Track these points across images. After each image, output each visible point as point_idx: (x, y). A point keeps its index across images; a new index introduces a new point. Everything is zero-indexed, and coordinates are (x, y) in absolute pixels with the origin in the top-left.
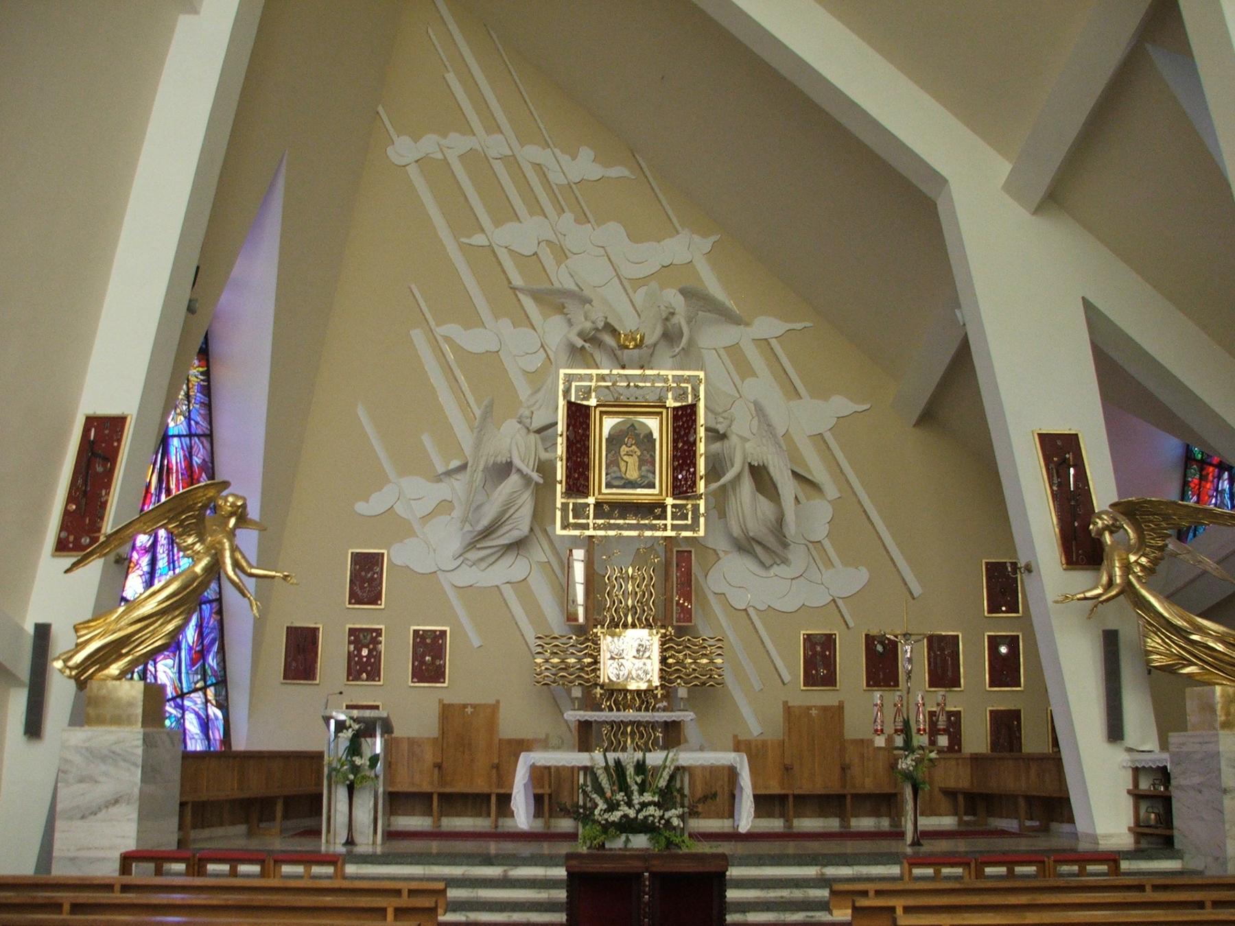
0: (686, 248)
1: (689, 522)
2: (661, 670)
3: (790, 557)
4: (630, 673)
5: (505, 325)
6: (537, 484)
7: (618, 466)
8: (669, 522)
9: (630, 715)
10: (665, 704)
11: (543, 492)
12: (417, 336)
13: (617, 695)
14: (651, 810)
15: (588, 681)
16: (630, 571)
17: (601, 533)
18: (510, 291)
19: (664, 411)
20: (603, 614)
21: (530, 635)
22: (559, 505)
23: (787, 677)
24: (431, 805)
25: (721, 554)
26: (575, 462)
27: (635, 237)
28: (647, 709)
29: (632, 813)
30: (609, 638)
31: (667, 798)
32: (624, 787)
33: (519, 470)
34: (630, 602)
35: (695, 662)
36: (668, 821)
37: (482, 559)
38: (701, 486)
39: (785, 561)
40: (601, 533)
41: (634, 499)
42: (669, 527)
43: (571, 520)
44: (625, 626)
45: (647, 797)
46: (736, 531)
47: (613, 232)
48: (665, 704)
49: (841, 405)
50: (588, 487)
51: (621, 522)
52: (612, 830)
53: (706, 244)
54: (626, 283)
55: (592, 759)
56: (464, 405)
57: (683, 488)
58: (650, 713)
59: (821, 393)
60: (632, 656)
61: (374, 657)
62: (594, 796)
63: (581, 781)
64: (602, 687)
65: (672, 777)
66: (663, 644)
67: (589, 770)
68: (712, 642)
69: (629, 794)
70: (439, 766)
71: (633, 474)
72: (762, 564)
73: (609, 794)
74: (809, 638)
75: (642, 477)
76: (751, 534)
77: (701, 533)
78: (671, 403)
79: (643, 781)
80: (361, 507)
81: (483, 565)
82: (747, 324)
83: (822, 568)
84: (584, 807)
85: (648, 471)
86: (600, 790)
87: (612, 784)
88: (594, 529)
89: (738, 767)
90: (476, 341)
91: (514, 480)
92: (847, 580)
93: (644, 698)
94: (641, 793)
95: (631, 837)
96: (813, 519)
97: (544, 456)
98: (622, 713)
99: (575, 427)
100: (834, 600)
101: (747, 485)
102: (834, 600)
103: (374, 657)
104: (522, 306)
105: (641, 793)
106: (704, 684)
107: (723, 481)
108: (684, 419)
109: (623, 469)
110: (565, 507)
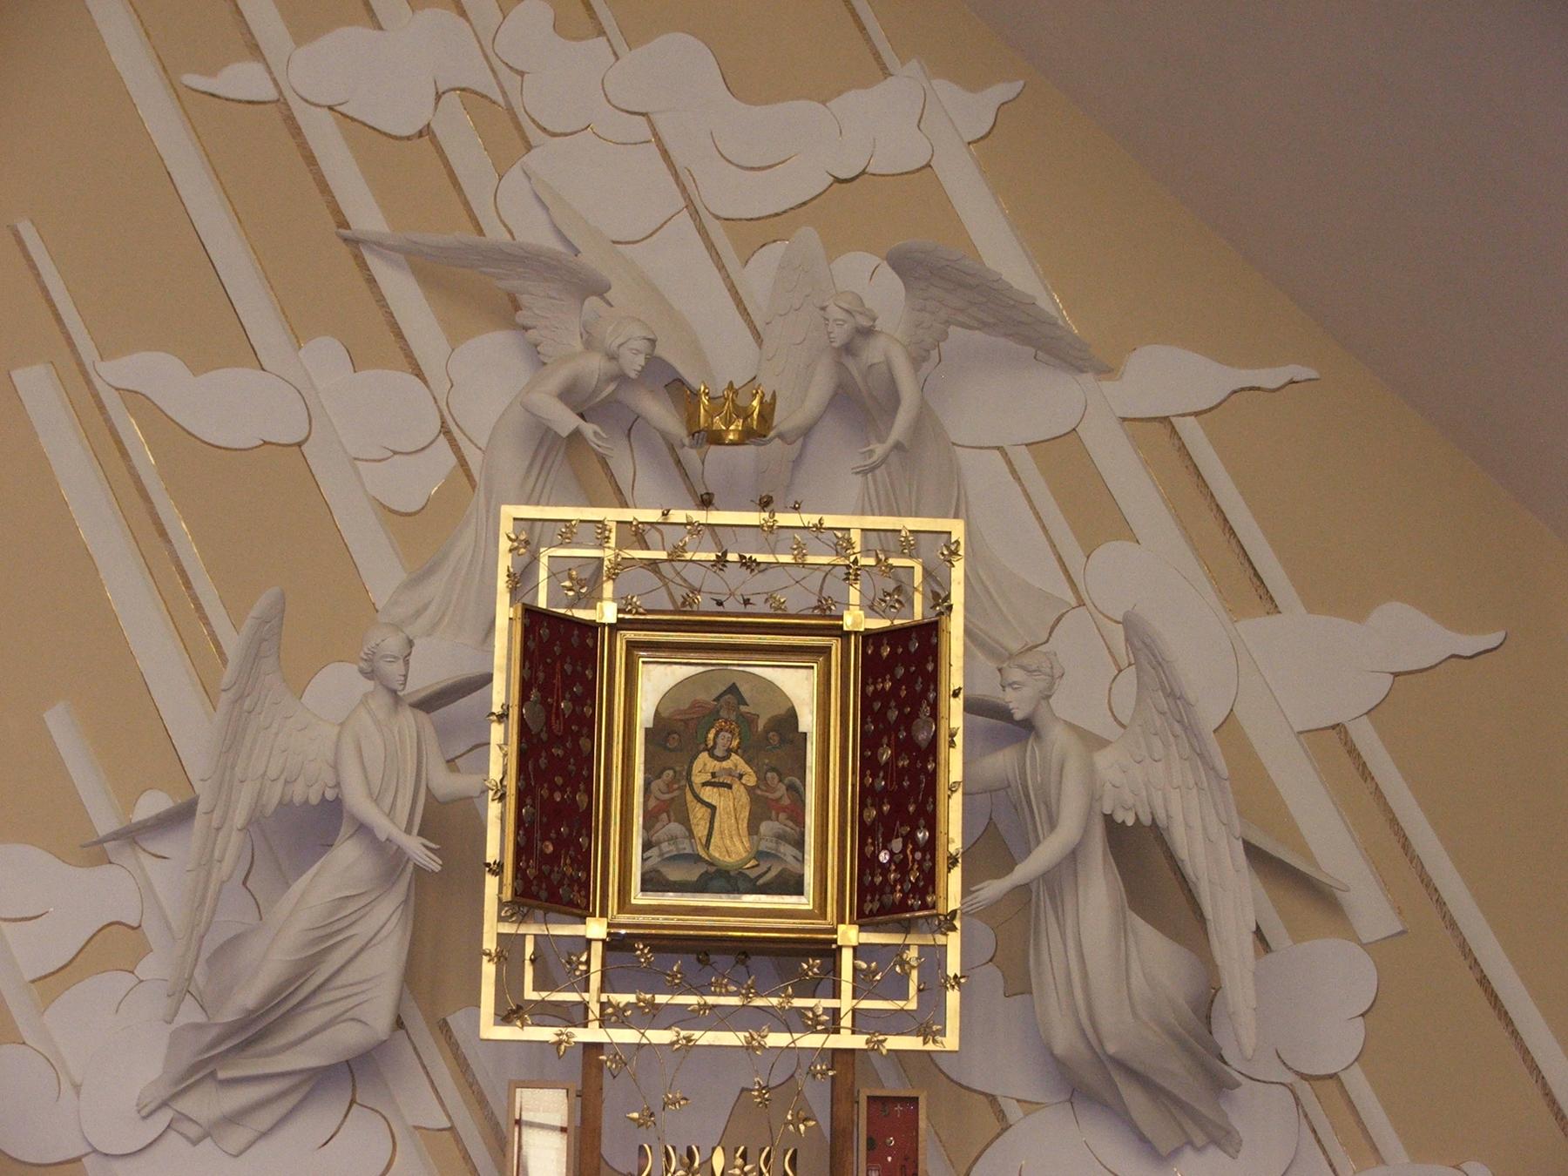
0: (910, 121)
3: (1237, 1123)
5: (325, 357)
7: (685, 821)
8: (846, 1003)
11: (438, 899)
12: (36, 385)
19: (835, 644)
22: (490, 944)
33: (363, 829)
37: (234, 1119)
38: (952, 886)
42: (846, 1021)
43: (530, 994)
47: (679, 67)
49: (1409, 635)
50: (585, 886)
53: (975, 110)
54: (716, 230)
56: (201, 650)
57: (892, 888)
59: (1340, 592)
71: (731, 847)
75: (760, 855)
76: (1111, 1048)
81: (238, 1137)
82: (1106, 371)
88: (604, 1022)
90: (227, 408)
91: (347, 854)
97: (446, 783)
99: (546, 690)
101: (1099, 890)
107: (1024, 871)
108: (898, 672)
109: (700, 831)
110: (509, 949)
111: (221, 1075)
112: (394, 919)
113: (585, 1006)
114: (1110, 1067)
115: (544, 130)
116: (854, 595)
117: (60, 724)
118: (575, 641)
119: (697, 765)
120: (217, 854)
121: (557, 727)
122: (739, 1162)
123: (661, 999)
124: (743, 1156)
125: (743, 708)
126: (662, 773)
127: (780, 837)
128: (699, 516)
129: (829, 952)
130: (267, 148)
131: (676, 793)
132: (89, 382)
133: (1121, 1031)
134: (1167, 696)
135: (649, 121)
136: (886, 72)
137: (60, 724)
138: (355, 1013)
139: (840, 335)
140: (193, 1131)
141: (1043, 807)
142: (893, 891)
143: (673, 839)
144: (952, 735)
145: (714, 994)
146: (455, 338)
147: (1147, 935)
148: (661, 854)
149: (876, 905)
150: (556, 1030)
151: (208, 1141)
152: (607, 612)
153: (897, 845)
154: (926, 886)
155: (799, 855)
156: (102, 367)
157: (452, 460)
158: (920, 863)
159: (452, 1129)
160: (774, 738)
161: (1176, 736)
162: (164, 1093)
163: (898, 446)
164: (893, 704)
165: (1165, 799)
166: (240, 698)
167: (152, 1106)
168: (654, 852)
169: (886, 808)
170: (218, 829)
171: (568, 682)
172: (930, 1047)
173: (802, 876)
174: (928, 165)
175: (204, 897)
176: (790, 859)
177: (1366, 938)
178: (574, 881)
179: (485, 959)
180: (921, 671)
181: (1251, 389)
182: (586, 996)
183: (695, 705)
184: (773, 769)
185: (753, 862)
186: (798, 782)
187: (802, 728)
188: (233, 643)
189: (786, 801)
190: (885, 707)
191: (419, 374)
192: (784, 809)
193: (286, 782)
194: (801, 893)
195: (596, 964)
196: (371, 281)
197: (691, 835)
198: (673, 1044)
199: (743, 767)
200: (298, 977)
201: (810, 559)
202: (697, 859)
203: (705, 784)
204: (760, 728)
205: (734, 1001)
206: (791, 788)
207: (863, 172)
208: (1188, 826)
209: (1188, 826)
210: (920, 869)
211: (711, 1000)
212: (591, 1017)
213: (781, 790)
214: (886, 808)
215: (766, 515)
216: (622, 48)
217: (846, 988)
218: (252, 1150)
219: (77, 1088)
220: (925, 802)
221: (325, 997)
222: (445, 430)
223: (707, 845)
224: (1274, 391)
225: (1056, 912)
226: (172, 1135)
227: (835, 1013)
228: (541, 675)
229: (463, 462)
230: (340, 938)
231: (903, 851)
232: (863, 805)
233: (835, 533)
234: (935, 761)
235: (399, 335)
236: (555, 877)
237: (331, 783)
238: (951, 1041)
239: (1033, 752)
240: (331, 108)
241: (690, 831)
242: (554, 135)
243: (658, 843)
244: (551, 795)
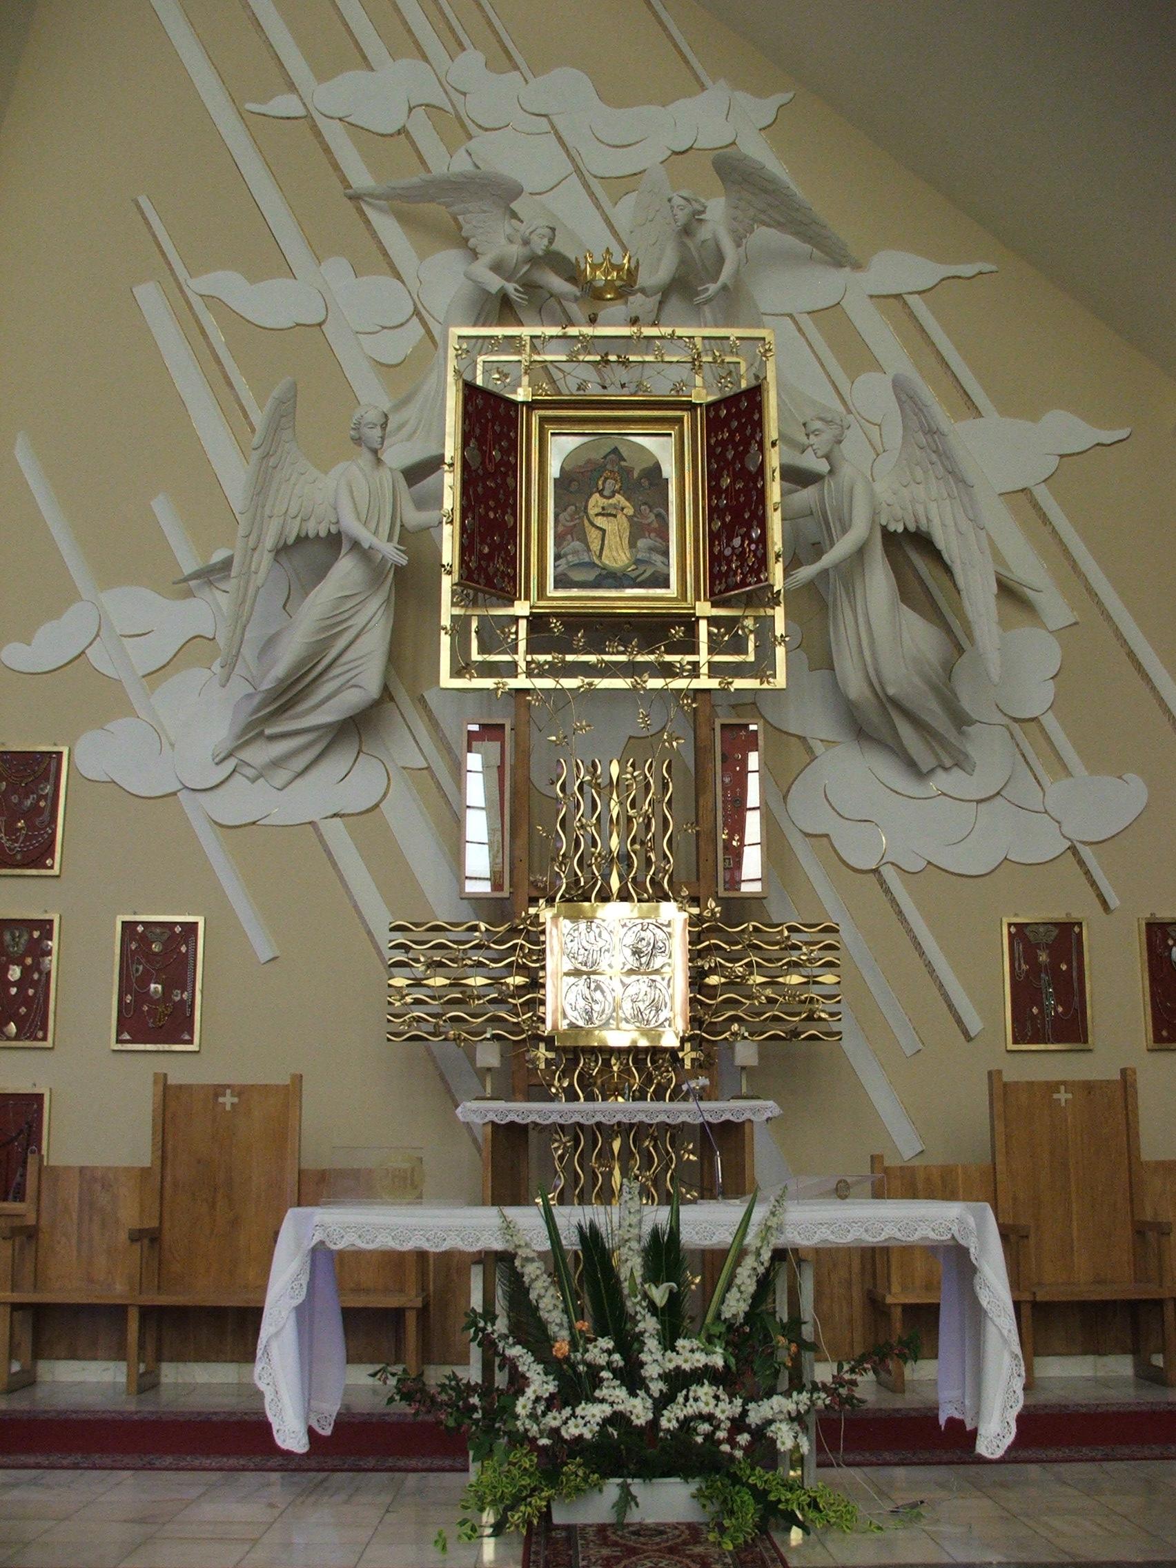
0: (725, 117)
1: (751, 658)
2: (693, 1001)
3: (970, 749)
4: (617, 1007)
5: (337, 271)
6: (398, 569)
7: (584, 540)
8: (703, 657)
9: (618, 1109)
10: (703, 1081)
11: (409, 585)
12: (149, 296)
13: (583, 1062)
14: (704, 1397)
15: (516, 1029)
16: (615, 769)
17: (547, 683)
18: (349, 204)
19: (686, 416)
20: (544, 869)
21: (380, 918)
22: (446, 621)
23: (974, 1024)
24: (123, 1332)
25: (819, 748)
26: (484, 519)
27: (614, 93)
28: (658, 1096)
29: (639, 1409)
30: (566, 925)
31: (754, 1355)
32: (610, 1317)
33: (356, 545)
34: (614, 843)
35: (772, 984)
36: (760, 1434)
37: (276, 763)
38: (777, 575)
39: (961, 762)
40: (547, 683)
41: (623, 608)
42: (704, 670)
43: (475, 656)
44: (605, 897)
45: (690, 1354)
46: (855, 687)
47: (568, 90)
48: (703, 1081)
49: (1066, 430)
50: (513, 579)
51: (592, 658)
52: (573, 1468)
53: (766, 109)
54: (594, 183)
55: (508, 1228)
56: (234, 412)
57: (733, 567)
58: (666, 1105)
59: (1022, 403)
60: (617, 972)
61: (34, 984)
62: (516, 1351)
63: (476, 1301)
64: (549, 1041)
65: (765, 1284)
66: (695, 939)
67: (501, 1263)
68: (810, 934)
69: (628, 1345)
70: (149, 1238)
71: (617, 556)
72: (911, 766)
73: (561, 1348)
74: (1020, 933)
75: (638, 562)
76: (891, 691)
77: (780, 681)
78: (701, 394)
79: (674, 1298)
80: (18, 656)
81: (282, 776)
82: (857, 266)
83: (1045, 779)
84: (486, 1389)
85: (651, 549)
86: (529, 1328)
87: (573, 1311)
88: (529, 674)
89: (972, 1245)
90: (271, 303)
91: (346, 568)
92: (1102, 804)
93: (647, 1060)
94: (668, 1344)
95: (636, 1486)
96: (1021, 666)
97: (414, 517)
98: (599, 1105)
99: (481, 441)
100: (1073, 849)
101: (879, 581)
102: (1073, 849)
103: (34, 984)
104: (374, 235)
105: (668, 1344)
106: (795, 1034)
107: (827, 560)
108: (733, 425)
109: (595, 546)
110: (459, 626)
111: (268, 732)
112: (380, 613)
113: (515, 664)
114: (888, 706)
115: (480, 127)
116: (698, 380)
117: (161, 507)
118: (502, 410)
119: (592, 502)
120: (253, 569)
121: (491, 468)
122: (630, 769)
123: (569, 658)
124: (633, 765)
125: (623, 463)
127: (651, 549)
128: (588, 331)
129: (690, 622)
130: (300, 145)
132: (182, 291)
133: (900, 679)
134: (925, 434)
136: (703, 87)
137: (161, 507)
139: (682, 216)
140: (250, 772)
141: (838, 524)
142: (735, 574)
143: (575, 552)
144: (774, 471)
145: (608, 653)
146: (422, 257)
147: (910, 617)
148: (568, 562)
149: (723, 587)
150: (496, 680)
151: (262, 780)
152: (522, 395)
153: (737, 542)
154: (760, 567)
155: (665, 560)
156: (191, 282)
157: (423, 331)
158: (755, 552)
159: (428, 768)
160: (645, 483)
161: (932, 464)
162: (229, 745)
163: (725, 288)
165: (926, 508)
166: (267, 456)
167: (221, 756)
168: (563, 561)
169: (728, 519)
170: (254, 550)
171: (498, 437)
172: (765, 686)
174: (734, 143)
175: (245, 595)
176: (659, 564)
177: (1052, 627)
178: (504, 575)
179: (443, 632)
180: (750, 419)
181: (953, 277)
182: (516, 657)
183: (589, 461)
184: (645, 504)
185: (633, 567)
186: (662, 511)
187: (665, 475)
188: (258, 417)
189: (655, 525)
190: (723, 453)
191: (399, 277)
192: (655, 530)
193: (303, 520)
194: (668, 587)
195: (523, 634)
196: (367, 222)
197: (589, 550)
198: (579, 688)
201: (667, 359)
202: (594, 565)
203: (597, 515)
204: (635, 475)
205: (623, 658)
206: (658, 516)
208: (944, 525)
209: (944, 525)
210: (755, 556)
211: (607, 658)
213: (652, 517)
214: (728, 519)
215: (635, 329)
216: (529, 75)
217: (704, 647)
218: (293, 785)
219: (172, 745)
220: (757, 508)
221: (335, 671)
222: (417, 312)
223: (600, 556)
224: (969, 278)
225: (847, 593)
226: (237, 776)
227: (695, 665)
228: (478, 431)
229: (429, 332)
230: (345, 626)
231: (742, 545)
233: (683, 356)
234: (763, 479)
235: (385, 254)
236: (491, 570)
237: (334, 520)
238: (780, 681)
239: (829, 485)
240: (340, 119)
241: (588, 547)
243: (565, 555)
244: (487, 513)
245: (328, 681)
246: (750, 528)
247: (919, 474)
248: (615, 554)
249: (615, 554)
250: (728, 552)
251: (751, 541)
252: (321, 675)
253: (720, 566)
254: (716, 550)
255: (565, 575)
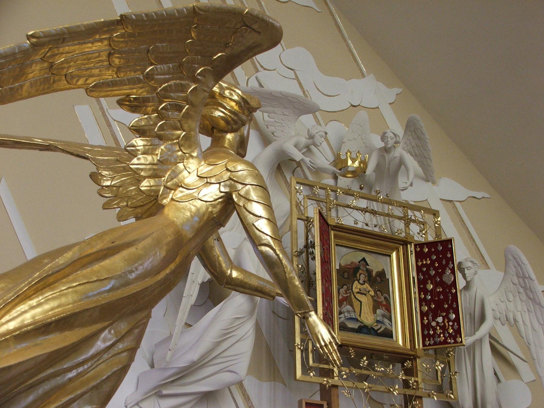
7: (352, 305)
27: (326, 68)
75: (378, 322)
109: (357, 310)
125: (368, 267)
126: (343, 286)
131: (348, 295)
134: (518, 277)
135: (295, 72)
138: (230, 368)
142: (439, 336)
143: (348, 312)
148: (345, 317)
149: (432, 342)
153: (440, 319)
160: (378, 279)
164: (432, 269)
168: (342, 315)
173: (392, 331)
183: (352, 263)
185: (376, 324)
189: (384, 303)
192: (384, 305)
197: (355, 311)
199: (369, 288)
200: (211, 350)
202: (357, 320)
203: (358, 293)
206: (385, 298)
207: (359, 105)
212: (335, 375)
213: (383, 299)
220: (452, 303)
223: (360, 316)
231: (443, 322)
232: (421, 305)
241: (353, 308)
242: (265, 69)
243: (344, 313)
245: (210, 366)
246: (448, 313)
247: (511, 298)
248: (367, 316)
249: (367, 316)
250: (434, 324)
251: (449, 320)
252: (206, 363)
253: (429, 331)
254: (426, 322)
255: (344, 323)
